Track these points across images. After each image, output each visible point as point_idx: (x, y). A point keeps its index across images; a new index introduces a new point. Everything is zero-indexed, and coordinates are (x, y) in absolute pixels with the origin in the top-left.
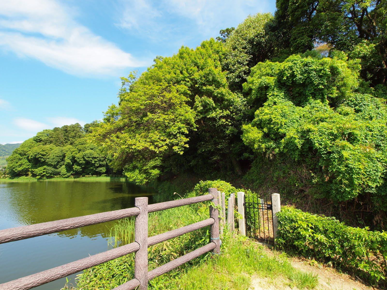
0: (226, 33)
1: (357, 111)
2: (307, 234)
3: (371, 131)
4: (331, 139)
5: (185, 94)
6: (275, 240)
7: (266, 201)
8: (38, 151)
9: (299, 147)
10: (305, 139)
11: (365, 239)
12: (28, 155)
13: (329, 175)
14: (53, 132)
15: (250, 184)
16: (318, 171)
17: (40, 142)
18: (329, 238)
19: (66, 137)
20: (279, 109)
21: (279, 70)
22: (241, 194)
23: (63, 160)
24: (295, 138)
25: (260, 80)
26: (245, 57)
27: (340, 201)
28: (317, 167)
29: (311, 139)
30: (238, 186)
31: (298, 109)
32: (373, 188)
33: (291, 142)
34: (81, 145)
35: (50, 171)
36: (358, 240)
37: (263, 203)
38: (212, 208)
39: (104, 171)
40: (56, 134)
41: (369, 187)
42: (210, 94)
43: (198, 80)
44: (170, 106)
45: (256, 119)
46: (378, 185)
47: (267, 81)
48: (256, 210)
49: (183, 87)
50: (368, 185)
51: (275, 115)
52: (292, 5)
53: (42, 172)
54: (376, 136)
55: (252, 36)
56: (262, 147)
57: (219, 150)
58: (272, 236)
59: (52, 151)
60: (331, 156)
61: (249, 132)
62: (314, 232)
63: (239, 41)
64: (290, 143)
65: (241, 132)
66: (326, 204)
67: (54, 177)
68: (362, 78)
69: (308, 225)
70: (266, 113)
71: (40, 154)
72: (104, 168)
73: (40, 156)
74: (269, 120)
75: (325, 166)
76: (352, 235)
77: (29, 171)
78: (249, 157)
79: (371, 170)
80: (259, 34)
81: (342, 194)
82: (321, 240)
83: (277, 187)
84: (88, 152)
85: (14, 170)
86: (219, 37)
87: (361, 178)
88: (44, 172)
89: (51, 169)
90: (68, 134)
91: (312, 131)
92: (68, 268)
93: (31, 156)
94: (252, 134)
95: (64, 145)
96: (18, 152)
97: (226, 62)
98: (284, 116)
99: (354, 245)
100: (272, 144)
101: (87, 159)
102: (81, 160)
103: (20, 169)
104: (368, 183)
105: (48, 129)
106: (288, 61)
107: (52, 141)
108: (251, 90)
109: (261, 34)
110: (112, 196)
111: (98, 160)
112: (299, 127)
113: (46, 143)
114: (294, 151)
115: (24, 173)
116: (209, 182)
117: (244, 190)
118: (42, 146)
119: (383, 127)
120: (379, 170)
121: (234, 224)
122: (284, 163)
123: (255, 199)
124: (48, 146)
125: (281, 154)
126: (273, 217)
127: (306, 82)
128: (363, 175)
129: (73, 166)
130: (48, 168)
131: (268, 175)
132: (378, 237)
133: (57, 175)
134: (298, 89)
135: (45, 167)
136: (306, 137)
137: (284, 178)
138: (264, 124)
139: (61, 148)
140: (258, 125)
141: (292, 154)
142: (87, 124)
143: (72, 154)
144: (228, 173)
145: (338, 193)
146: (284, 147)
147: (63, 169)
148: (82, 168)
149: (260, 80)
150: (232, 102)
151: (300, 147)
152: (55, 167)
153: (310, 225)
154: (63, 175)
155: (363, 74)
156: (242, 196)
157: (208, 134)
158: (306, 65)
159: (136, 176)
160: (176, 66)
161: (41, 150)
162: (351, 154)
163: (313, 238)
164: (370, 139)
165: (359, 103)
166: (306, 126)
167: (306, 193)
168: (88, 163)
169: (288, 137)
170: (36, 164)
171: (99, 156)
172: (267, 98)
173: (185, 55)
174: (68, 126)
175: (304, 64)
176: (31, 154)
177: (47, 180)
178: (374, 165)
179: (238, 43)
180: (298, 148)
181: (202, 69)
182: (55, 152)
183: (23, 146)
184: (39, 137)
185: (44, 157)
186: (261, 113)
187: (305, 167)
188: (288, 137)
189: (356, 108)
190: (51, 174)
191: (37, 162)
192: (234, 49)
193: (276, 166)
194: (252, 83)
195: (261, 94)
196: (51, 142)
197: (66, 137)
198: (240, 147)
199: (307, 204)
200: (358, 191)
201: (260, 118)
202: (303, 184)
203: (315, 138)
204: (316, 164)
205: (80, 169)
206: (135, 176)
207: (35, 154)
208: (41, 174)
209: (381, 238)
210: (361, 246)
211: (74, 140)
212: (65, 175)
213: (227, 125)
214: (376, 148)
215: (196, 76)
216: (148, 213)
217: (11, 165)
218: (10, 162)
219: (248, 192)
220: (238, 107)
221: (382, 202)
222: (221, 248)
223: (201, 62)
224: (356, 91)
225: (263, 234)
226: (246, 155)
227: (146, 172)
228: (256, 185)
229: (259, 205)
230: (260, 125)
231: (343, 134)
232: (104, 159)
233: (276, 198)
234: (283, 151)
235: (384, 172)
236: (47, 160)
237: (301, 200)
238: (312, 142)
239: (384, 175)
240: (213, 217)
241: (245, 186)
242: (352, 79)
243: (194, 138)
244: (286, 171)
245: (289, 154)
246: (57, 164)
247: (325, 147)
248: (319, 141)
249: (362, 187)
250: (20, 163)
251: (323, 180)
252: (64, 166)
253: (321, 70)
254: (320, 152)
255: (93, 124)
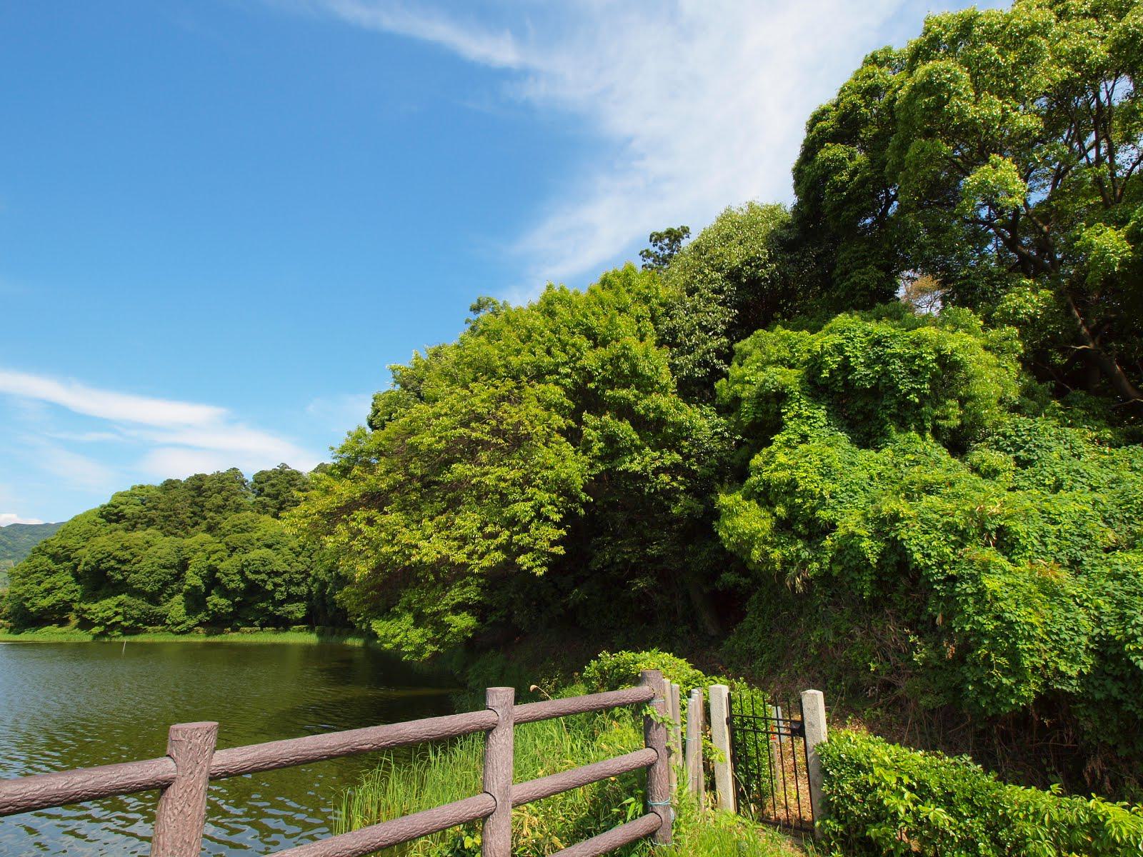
0: (667, 241)
1: (1023, 464)
2: (901, 804)
3: (1055, 523)
4: (953, 542)
5: (560, 408)
6: (817, 824)
7: (789, 711)
8: (109, 549)
9: (873, 560)
10: (886, 540)
11: (1050, 817)
12: (76, 561)
13: (956, 641)
14: (160, 494)
15: (744, 664)
16: (926, 628)
17: (117, 521)
18: (959, 817)
19: (197, 509)
20: (811, 453)
21: (809, 351)
22: (720, 690)
23: (178, 577)
24: (860, 537)
25: (761, 376)
26: (719, 315)
27: (990, 714)
28: (924, 617)
29: (903, 540)
30: (711, 669)
31: (864, 455)
32: (1071, 678)
33: (851, 546)
34: (238, 532)
35: (135, 613)
36: (1034, 821)
37: (780, 717)
38: (651, 720)
39: (300, 615)
40: (170, 499)
41: (1062, 675)
42: (624, 411)
43: (597, 370)
44: (518, 442)
45: (754, 479)
46: (1085, 671)
47: (780, 378)
48: (761, 737)
49: (554, 392)
50: (1057, 669)
51: (806, 471)
52: (832, 193)
53: (110, 613)
54: (1067, 535)
55: (736, 263)
56: (773, 556)
57: (652, 560)
58: (808, 816)
59: (151, 550)
60: (957, 590)
61: (737, 515)
62: (917, 800)
63: (703, 273)
64: (848, 547)
65: (714, 514)
66: (957, 724)
67: (145, 631)
68: (1029, 374)
69: (900, 780)
70: (781, 465)
71: (114, 558)
72: (302, 606)
73: (113, 563)
74: (788, 485)
75: (943, 616)
76: (1016, 807)
77: (72, 610)
78: (737, 585)
79: (1063, 628)
80: (753, 259)
81: (994, 694)
82: (936, 821)
83: (820, 672)
84: (255, 554)
85: (27, 604)
86: (647, 251)
87: (1038, 650)
88: (117, 614)
89: (139, 606)
90: (201, 500)
91: (903, 519)
92: (364, 838)
93: (86, 564)
94: (745, 519)
95: (187, 533)
96: (49, 550)
97: (671, 325)
98: (827, 472)
99: (1024, 837)
100: (800, 548)
101: (251, 576)
102: (233, 581)
103: (45, 603)
104: (1057, 663)
105: (145, 484)
106: (831, 331)
107: (154, 521)
108: (737, 400)
109: (760, 259)
110: (326, 693)
111: (284, 580)
112: (870, 508)
113: (134, 526)
114: (858, 570)
115: (56, 615)
116: (627, 656)
117: (726, 681)
118: (121, 533)
119: (1085, 512)
120: (1082, 630)
121: (703, 779)
122: (836, 604)
123: (758, 706)
124: (139, 535)
125: (825, 578)
126: (809, 756)
127: (881, 385)
128: (1042, 641)
129: (208, 599)
130: (131, 603)
131: (793, 639)
132: (1081, 813)
133: (155, 625)
134: (860, 404)
135: (123, 597)
136: (887, 534)
137: (836, 646)
138: (777, 495)
139: (178, 541)
140: (760, 494)
141: (853, 580)
142: (262, 473)
143: (208, 559)
144: (679, 630)
145: (981, 693)
146: (833, 560)
147: (175, 608)
148: (234, 604)
149: (761, 376)
150: (687, 429)
151: (875, 561)
152: (153, 598)
153: (906, 780)
154: (173, 624)
155: (1034, 363)
156: (721, 696)
157: (621, 516)
158: (877, 342)
159: (402, 634)
160: (535, 336)
161: (118, 546)
162: (1007, 585)
163: (916, 815)
164: (1054, 544)
165: (1026, 442)
166: (890, 505)
167: (899, 692)
168: (254, 590)
169: (841, 532)
170: (96, 589)
171: (288, 568)
172: (783, 423)
173: (558, 308)
174: (206, 476)
175: (872, 340)
176: (86, 556)
177: (126, 639)
178: (1069, 616)
179: (700, 277)
180: (870, 565)
181: (605, 343)
182: (158, 554)
183: (65, 530)
184: (116, 507)
185: (123, 568)
186: (767, 463)
187: (891, 617)
188: (841, 532)
189: (1018, 454)
190: (137, 620)
191: (99, 581)
192: (691, 293)
193: (813, 612)
194: (741, 380)
195: (766, 412)
196: (151, 522)
197: (197, 509)
198: (713, 556)
199: (904, 724)
200: (1033, 687)
201: (765, 475)
202: (887, 666)
203: (913, 539)
204: (920, 610)
205: (228, 606)
206: (399, 633)
207: (100, 556)
208: (109, 619)
209: (1090, 815)
210: (1043, 838)
211: (218, 518)
212: (179, 624)
213: (675, 490)
214: (1070, 567)
215: (590, 359)
216: (515, 724)
217: (20, 590)
218: (18, 580)
219: (737, 685)
220: (703, 444)
221: (1100, 718)
222: (674, 831)
223: (599, 324)
224: (1015, 409)
225: (783, 811)
226: (729, 577)
227: (441, 627)
228: (762, 668)
229: (770, 722)
230: (765, 496)
231: (983, 530)
232: (304, 579)
233: (814, 701)
234: (830, 569)
235: (1094, 634)
236: (132, 575)
237: (888, 711)
238: (905, 548)
239: (1097, 642)
240: (654, 746)
241: (729, 670)
242: (993, 371)
243: (583, 528)
244: (843, 627)
245: (848, 579)
246: (161, 591)
247: (940, 565)
248: (923, 548)
249: (1042, 675)
250: (49, 586)
251: (941, 656)
252: (179, 598)
253: (914, 357)
254: (928, 575)
255: (281, 473)
